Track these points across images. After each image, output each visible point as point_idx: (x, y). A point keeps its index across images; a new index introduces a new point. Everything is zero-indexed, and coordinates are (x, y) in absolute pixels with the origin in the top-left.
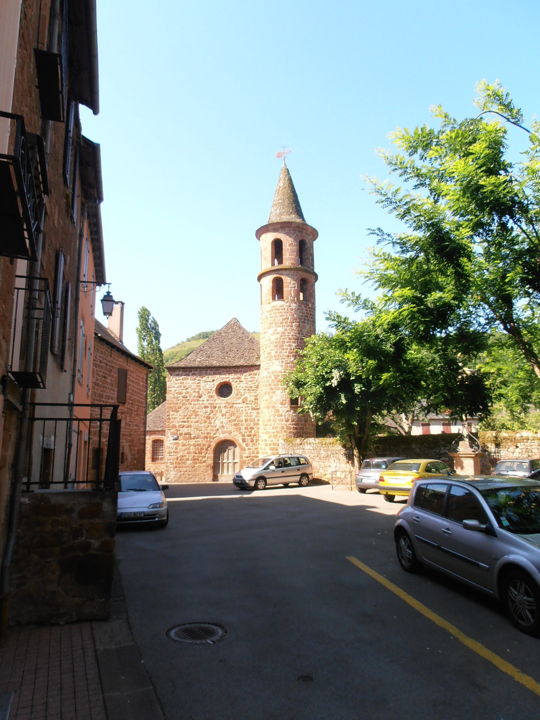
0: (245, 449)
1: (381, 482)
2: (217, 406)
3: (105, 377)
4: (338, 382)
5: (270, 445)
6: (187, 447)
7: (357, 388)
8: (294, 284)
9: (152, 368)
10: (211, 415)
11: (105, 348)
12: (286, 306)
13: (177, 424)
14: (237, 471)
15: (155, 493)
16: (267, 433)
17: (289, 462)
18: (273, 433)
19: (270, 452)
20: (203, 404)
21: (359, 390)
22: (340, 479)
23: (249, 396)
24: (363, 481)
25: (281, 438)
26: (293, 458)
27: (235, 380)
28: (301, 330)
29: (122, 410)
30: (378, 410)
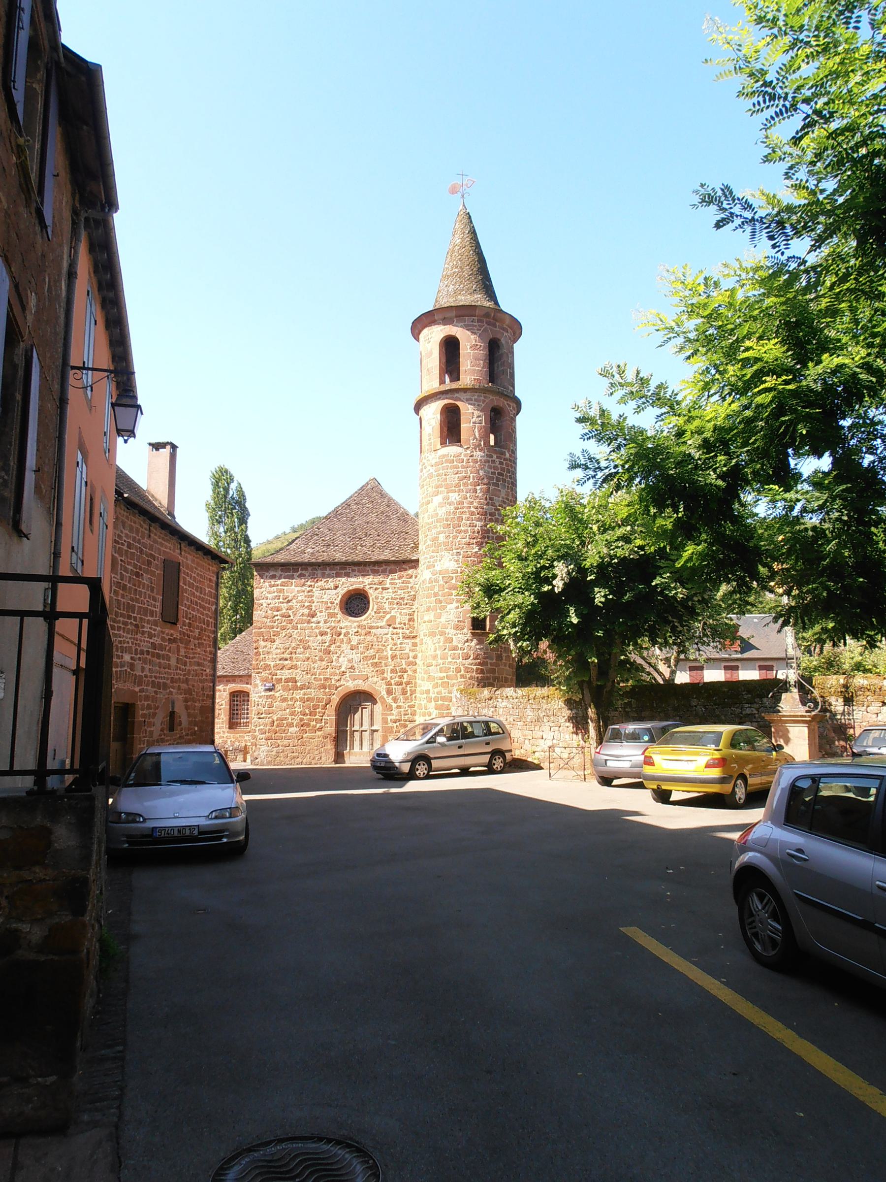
0: (391, 706)
1: (647, 767)
2: (343, 631)
3: (137, 575)
4: (565, 584)
5: (436, 700)
6: (290, 703)
7: (600, 596)
8: (478, 417)
9: (226, 562)
10: (332, 648)
11: (138, 522)
12: (465, 456)
13: (272, 664)
14: (377, 746)
15: (223, 789)
16: (430, 679)
17: (470, 730)
18: (441, 679)
19: (435, 713)
20: (317, 628)
21: (603, 600)
22: (563, 764)
23: (398, 615)
24: (609, 763)
25: (455, 688)
26: (478, 722)
27: (375, 586)
28: (490, 499)
29: (172, 635)
30: (633, 635)
